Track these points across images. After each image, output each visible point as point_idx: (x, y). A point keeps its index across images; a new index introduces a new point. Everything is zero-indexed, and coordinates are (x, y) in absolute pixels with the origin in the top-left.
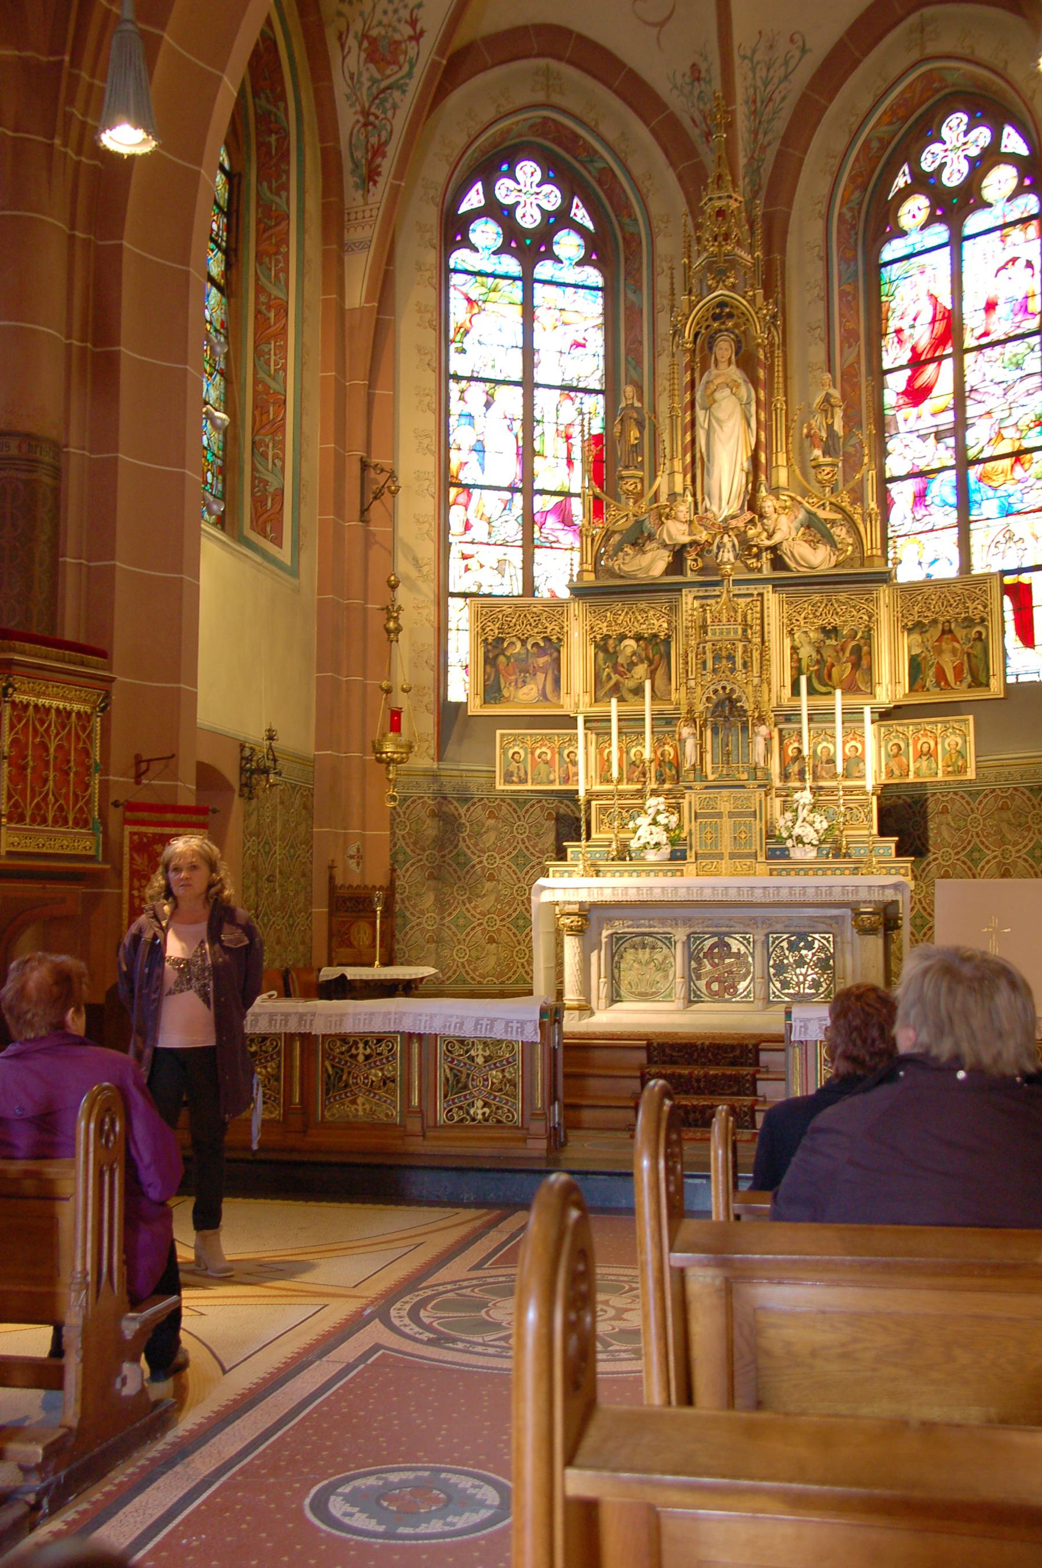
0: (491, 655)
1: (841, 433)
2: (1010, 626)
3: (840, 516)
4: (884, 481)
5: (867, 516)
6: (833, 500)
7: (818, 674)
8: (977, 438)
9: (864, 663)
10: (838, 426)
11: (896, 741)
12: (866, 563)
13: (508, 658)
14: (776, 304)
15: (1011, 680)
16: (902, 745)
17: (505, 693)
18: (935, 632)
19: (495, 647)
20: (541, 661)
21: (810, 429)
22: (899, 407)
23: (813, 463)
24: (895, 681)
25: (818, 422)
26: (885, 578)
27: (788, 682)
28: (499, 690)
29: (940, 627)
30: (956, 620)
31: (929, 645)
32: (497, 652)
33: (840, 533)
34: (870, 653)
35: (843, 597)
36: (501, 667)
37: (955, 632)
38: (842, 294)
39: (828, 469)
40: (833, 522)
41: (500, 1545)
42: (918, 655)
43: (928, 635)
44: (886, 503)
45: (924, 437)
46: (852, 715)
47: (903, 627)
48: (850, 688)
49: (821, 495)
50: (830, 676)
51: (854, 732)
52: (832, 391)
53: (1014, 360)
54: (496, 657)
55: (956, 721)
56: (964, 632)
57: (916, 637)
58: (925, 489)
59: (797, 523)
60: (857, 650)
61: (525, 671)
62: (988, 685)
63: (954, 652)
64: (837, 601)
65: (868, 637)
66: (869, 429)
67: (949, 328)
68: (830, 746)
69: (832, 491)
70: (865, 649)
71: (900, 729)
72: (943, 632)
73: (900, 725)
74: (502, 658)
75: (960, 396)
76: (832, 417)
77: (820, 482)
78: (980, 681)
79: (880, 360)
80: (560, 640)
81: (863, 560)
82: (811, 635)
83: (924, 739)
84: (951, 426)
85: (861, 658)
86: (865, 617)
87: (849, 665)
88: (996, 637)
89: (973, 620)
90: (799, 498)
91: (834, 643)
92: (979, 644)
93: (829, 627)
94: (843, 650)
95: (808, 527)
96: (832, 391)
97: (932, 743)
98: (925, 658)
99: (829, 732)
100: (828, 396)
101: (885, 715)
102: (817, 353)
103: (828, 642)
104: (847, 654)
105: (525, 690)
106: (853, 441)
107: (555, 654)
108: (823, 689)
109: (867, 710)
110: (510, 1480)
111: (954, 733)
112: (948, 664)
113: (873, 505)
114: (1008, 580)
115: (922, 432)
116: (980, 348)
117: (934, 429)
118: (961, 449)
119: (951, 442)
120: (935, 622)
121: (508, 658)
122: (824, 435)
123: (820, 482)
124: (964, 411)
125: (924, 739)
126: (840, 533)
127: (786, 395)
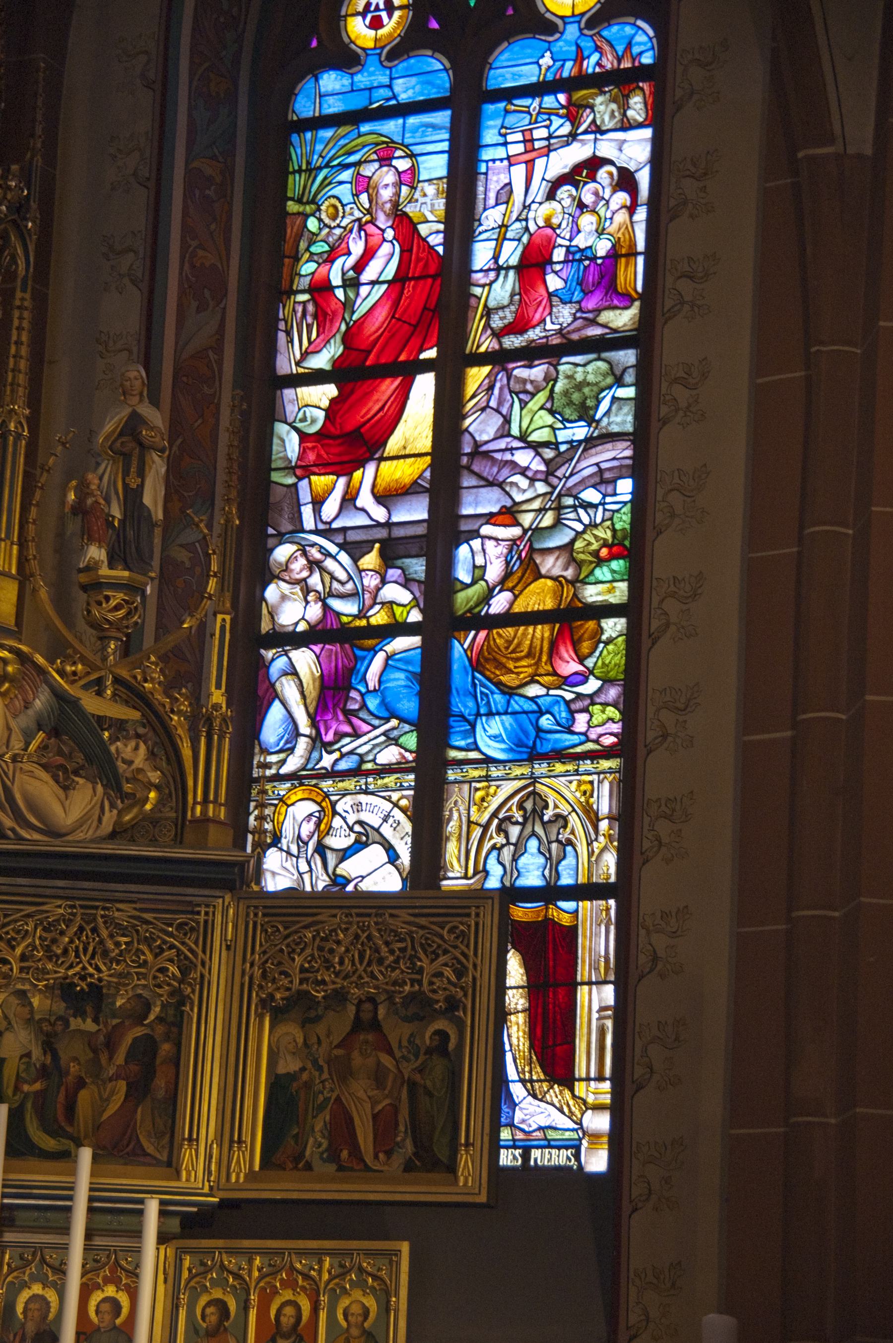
1: (159, 515)
2: (517, 1033)
3: (135, 715)
4: (257, 640)
5: (200, 721)
6: (124, 674)
7: (42, 1100)
8: (482, 557)
9: (160, 1083)
10: (152, 497)
11: (217, 1294)
12: (189, 836)
14: (26, 178)
15: (507, 1158)
16: (232, 1305)
18: (338, 1024)
21: (83, 490)
22: (304, 470)
23: (83, 578)
24: (230, 1136)
25: (104, 477)
26: (238, 877)
29: (352, 1009)
30: (390, 998)
31: (322, 1053)
33: (133, 754)
34: (176, 1061)
35: (123, 913)
37: (386, 1029)
38: (193, 178)
39: (118, 597)
40: (119, 727)
41: (127, 1332)
42: (292, 1077)
43: (321, 1029)
44: (254, 694)
45: (356, 550)
46: (114, 1221)
47: (263, 1003)
48: (117, 1149)
49: (96, 659)
50: (70, 1109)
51: (112, 1262)
52: (146, 410)
53: (576, 397)
55: (369, 1253)
56: (406, 1030)
57: (293, 1031)
58: (351, 671)
59: (26, 720)
60: (145, 1051)
62: (452, 1169)
63: (379, 1076)
64: (107, 921)
65: (175, 1022)
66: (228, 512)
67: (434, 288)
68: (52, 1296)
69: (126, 650)
70: (166, 1048)
71: (230, 1262)
72: (358, 1025)
73: (231, 1252)
75: (452, 459)
76: (141, 474)
77: (95, 625)
78: (434, 1160)
79: (272, 351)
81: (183, 828)
82: (36, 1001)
83: (288, 1295)
84: (421, 530)
85: (155, 1074)
87: (122, 1086)
88: (481, 1049)
89: (430, 1002)
90: (40, 660)
91: (89, 1026)
92: (439, 1066)
94: (111, 1045)
95: (55, 732)
96: (146, 410)
97: (306, 1306)
98: (308, 1085)
99: (52, 1257)
100: (135, 422)
101: (191, 1226)
102: (123, 314)
103: (75, 1023)
104: (120, 1058)
106: (189, 536)
108: (49, 1143)
109: (152, 1208)
111: (360, 1284)
112: (362, 1102)
113: (218, 697)
114: (522, 912)
115: (352, 536)
116: (500, 359)
117: (382, 533)
118: (438, 588)
119: (418, 567)
120: (339, 997)
122: (116, 512)
123: (95, 625)
124: (455, 500)
125: (288, 1295)
126: (133, 754)
127: (34, 401)
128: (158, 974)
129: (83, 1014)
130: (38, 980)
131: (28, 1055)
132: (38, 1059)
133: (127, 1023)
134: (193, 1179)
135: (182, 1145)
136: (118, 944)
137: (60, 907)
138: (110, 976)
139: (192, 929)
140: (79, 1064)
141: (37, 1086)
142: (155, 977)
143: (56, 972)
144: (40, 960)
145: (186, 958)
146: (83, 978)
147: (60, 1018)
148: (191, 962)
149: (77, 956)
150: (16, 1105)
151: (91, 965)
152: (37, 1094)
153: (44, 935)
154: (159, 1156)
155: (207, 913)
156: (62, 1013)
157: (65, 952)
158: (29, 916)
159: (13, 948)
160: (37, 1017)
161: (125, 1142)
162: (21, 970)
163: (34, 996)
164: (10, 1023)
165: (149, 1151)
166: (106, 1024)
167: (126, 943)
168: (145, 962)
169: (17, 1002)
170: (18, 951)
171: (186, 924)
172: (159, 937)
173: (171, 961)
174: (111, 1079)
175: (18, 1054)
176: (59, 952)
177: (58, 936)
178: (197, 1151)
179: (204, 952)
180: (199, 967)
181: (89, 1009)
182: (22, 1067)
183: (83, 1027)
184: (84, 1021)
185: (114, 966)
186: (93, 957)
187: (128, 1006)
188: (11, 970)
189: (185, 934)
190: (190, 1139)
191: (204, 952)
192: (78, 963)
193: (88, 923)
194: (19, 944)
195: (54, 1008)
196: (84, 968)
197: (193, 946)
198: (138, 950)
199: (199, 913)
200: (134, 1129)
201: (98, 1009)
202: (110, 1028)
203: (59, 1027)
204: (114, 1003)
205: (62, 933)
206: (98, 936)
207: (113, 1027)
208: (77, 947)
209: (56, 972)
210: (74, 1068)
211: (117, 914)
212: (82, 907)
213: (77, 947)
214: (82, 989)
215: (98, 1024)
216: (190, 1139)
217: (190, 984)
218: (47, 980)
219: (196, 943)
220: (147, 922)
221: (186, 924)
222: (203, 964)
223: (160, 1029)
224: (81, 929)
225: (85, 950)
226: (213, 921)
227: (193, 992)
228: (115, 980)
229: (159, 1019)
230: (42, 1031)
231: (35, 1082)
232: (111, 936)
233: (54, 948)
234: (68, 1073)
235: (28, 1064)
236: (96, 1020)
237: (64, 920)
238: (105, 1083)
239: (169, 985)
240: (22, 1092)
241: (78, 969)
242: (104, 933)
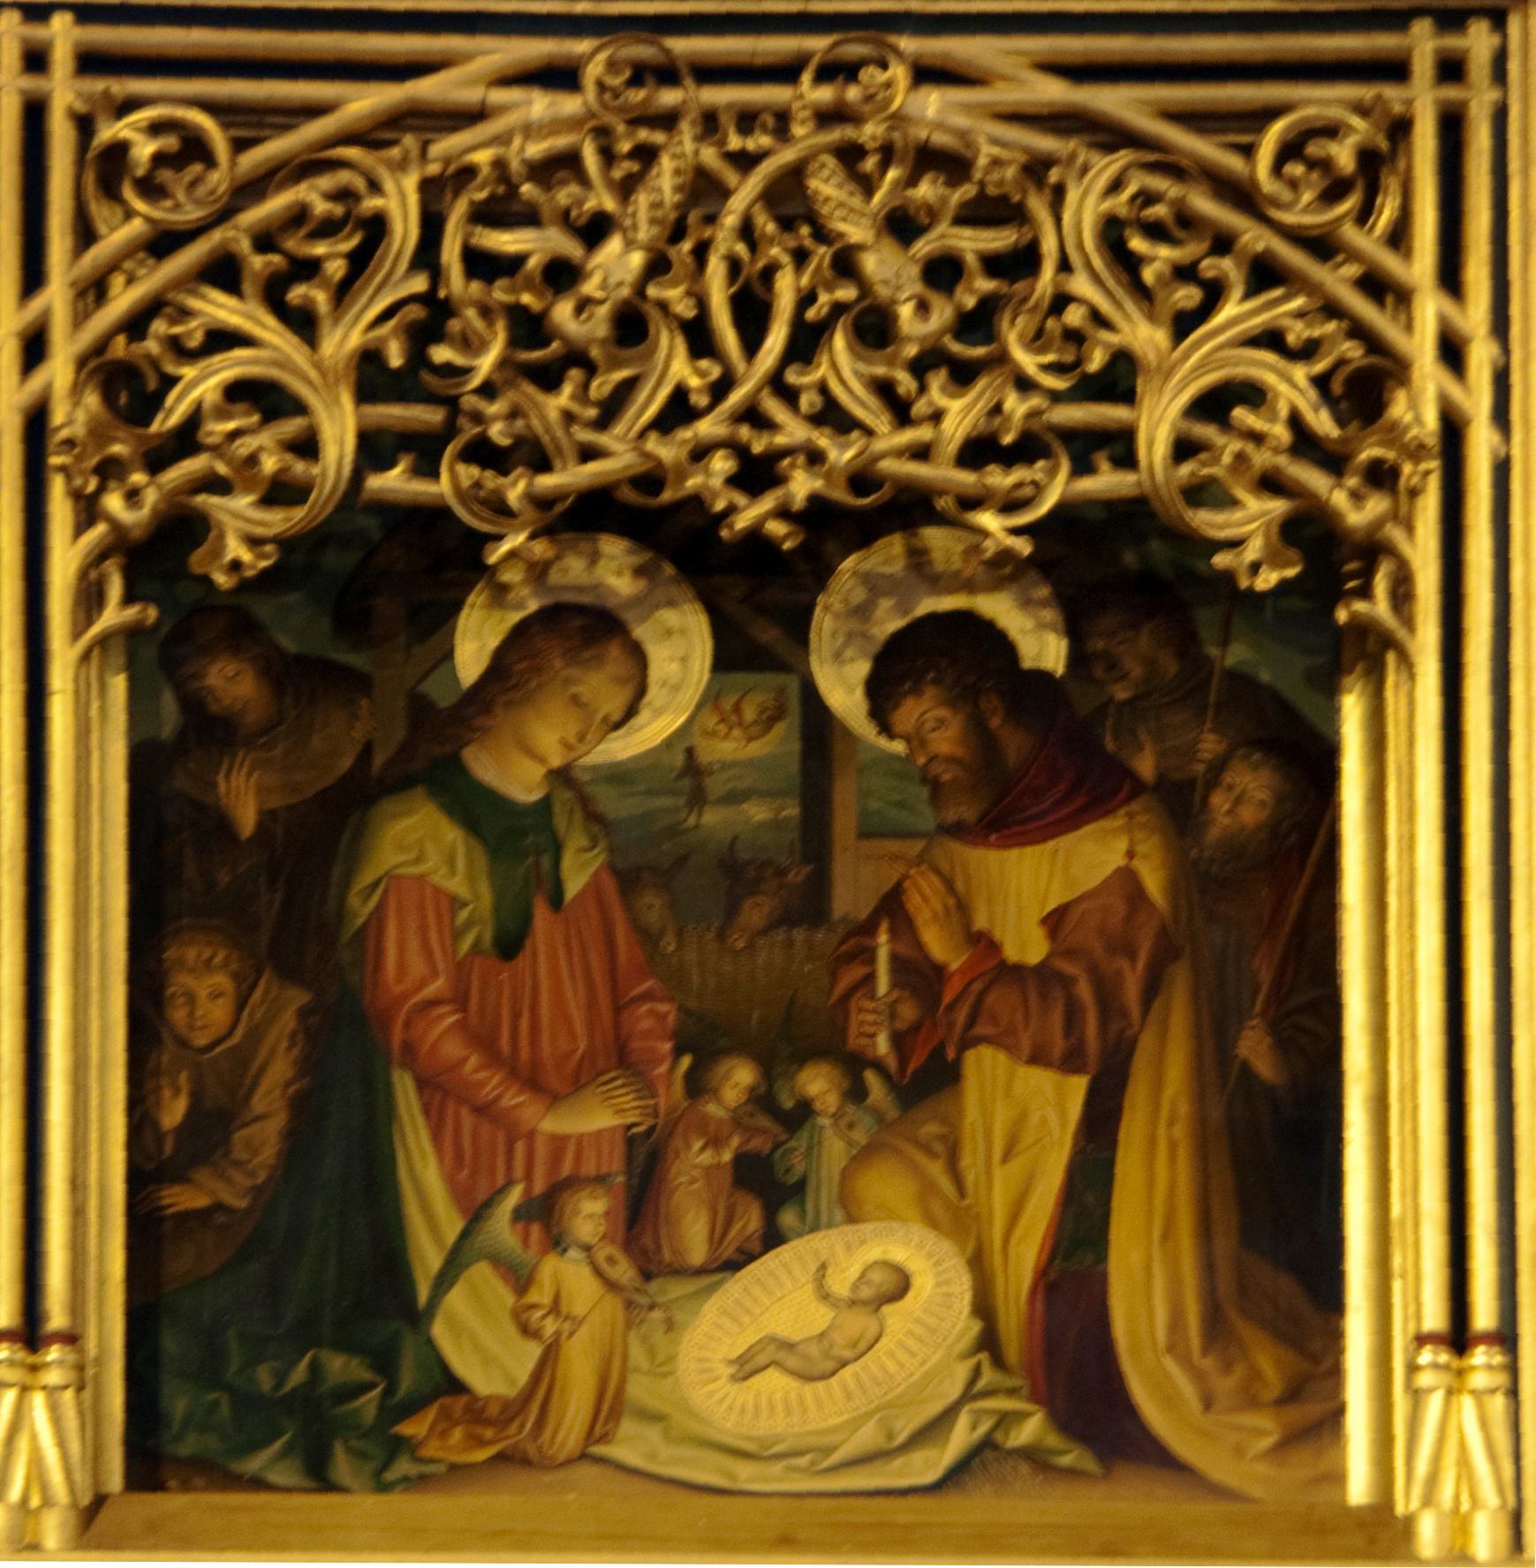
0: (245, 798)
13: (512, 838)
17: (476, 1337)
19: (301, 681)
20: (1030, 888)
28: (380, 1299)
32: (338, 742)
36: (410, 967)
54: (327, 827)
61: (773, 1021)
74: (415, 845)
80: (1330, 557)
105: (782, 1295)
107: (1246, 797)
121: (512, 838)
128: (1206, 431)
151: (789, 396)
155: (1451, 69)
167: (993, 264)
179: (1450, 278)
191: (1450, 278)
205: (595, 230)
209: (588, 454)
216: (1459, 1337)
219: (1399, 237)
232: (902, 226)
239: (1270, 484)
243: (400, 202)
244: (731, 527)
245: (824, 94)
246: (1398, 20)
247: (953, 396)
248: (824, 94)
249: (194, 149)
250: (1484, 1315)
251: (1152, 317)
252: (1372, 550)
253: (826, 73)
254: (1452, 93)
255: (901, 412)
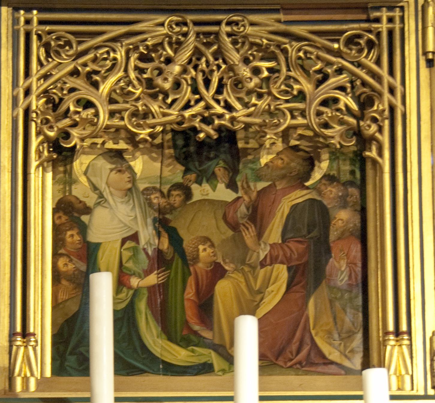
9: (340, 268)
27: (43, 321)
60: (312, 223)
70: (343, 218)
86: (347, 100)
87: (281, 272)
91: (223, 193)
93: (207, 132)
94: (257, 216)
103: (200, 191)
104: (274, 233)
108: (180, 355)
110: (286, 108)
128: (323, 109)
129: (212, 178)
130: (138, 126)
131: (135, 237)
132: (148, 243)
133: (280, 186)
134: (408, 386)
135: (383, 344)
136: (256, 71)
137: (162, 24)
138: (249, 115)
139: (371, 45)
140: (212, 245)
141: (152, 279)
142: (319, 114)
143: (165, 115)
144: (138, 99)
145: (364, 84)
146: (207, 121)
147: (177, 186)
148: (373, 89)
149: (195, 91)
150: (123, 305)
151: (218, 102)
152: (151, 289)
153: (142, 65)
154: (347, 363)
155: (390, 20)
156: (179, 179)
157: (177, 85)
158: (115, 40)
159: (96, 85)
160: (142, 186)
161: (294, 347)
162: (112, 114)
163: (134, 158)
164: (101, 196)
165: (331, 358)
166: (247, 190)
167: (270, 70)
168: (301, 93)
169: (109, 166)
170: (105, 88)
171: (359, 36)
172: (318, 58)
173: (342, 89)
174: (263, 264)
175: (119, 238)
176: (167, 86)
177: (163, 66)
178: (410, 346)
179: (391, 72)
180: (387, 96)
181: (220, 171)
182: (126, 255)
183: (213, 195)
184: (214, 188)
185: (254, 101)
186: (219, 90)
187: (280, 162)
188: (97, 115)
189: (360, 51)
190: (397, 333)
191: (391, 72)
192: (197, 101)
193: (208, 45)
194: (105, 78)
195: (167, 172)
196: (208, 107)
197: (375, 67)
198: (289, 77)
199: (378, 20)
200: (306, 328)
201: (233, 171)
202: (254, 195)
203: (177, 198)
204: (257, 160)
205: (169, 61)
206: (225, 62)
207: (259, 192)
208: (194, 80)
209: (165, 115)
210: (205, 253)
211: (250, 30)
212: (196, 23)
213: (194, 80)
214: (208, 136)
215: (235, 190)
216: (397, 333)
217: (375, 120)
218: (153, 127)
219: (378, 62)
220: (299, 38)
221: (359, 36)
222: (392, 91)
223: (332, 192)
224: (198, 54)
225: (207, 83)
226: (402, 30)
227: (380, 130)
228: (258, 120)
229: (329, 178)
230: (150, 204)
231: (147, 273)
232: (246, 61)
233: (159, 81)
234: (196, 259)
235: (135, 250)
236: (232, 185)
237: (170, 44)
238: (253, 268)
239: (341, 122)
240: (130, 288)
241: (199, 108)
242: (235, 57)
243: (120, 55)
244: (375, 144)
245: (228, 29)
246: (378, 8)
247: (259, 101)
248: (228, 29)
249: (68, 43)
250: (404, 327)
251: (309, 82)
252: (373, 138)
253: (229, 24)
254: (390, 26)
255: (246, 105)
